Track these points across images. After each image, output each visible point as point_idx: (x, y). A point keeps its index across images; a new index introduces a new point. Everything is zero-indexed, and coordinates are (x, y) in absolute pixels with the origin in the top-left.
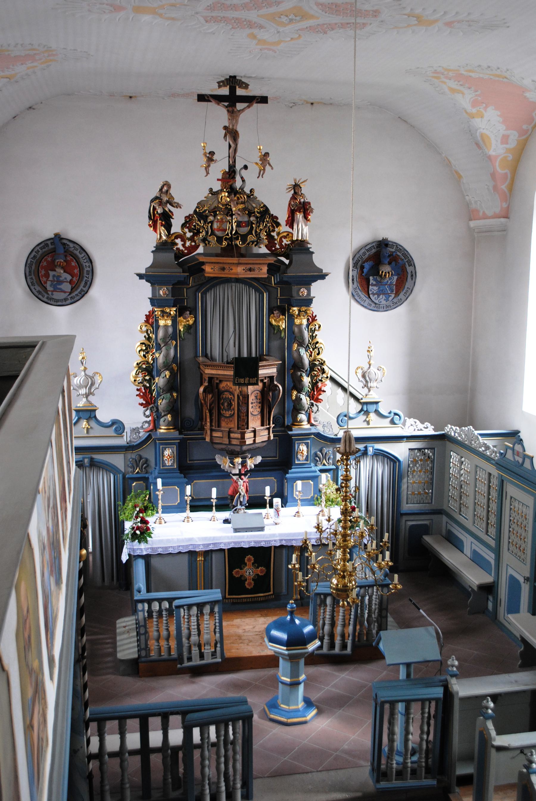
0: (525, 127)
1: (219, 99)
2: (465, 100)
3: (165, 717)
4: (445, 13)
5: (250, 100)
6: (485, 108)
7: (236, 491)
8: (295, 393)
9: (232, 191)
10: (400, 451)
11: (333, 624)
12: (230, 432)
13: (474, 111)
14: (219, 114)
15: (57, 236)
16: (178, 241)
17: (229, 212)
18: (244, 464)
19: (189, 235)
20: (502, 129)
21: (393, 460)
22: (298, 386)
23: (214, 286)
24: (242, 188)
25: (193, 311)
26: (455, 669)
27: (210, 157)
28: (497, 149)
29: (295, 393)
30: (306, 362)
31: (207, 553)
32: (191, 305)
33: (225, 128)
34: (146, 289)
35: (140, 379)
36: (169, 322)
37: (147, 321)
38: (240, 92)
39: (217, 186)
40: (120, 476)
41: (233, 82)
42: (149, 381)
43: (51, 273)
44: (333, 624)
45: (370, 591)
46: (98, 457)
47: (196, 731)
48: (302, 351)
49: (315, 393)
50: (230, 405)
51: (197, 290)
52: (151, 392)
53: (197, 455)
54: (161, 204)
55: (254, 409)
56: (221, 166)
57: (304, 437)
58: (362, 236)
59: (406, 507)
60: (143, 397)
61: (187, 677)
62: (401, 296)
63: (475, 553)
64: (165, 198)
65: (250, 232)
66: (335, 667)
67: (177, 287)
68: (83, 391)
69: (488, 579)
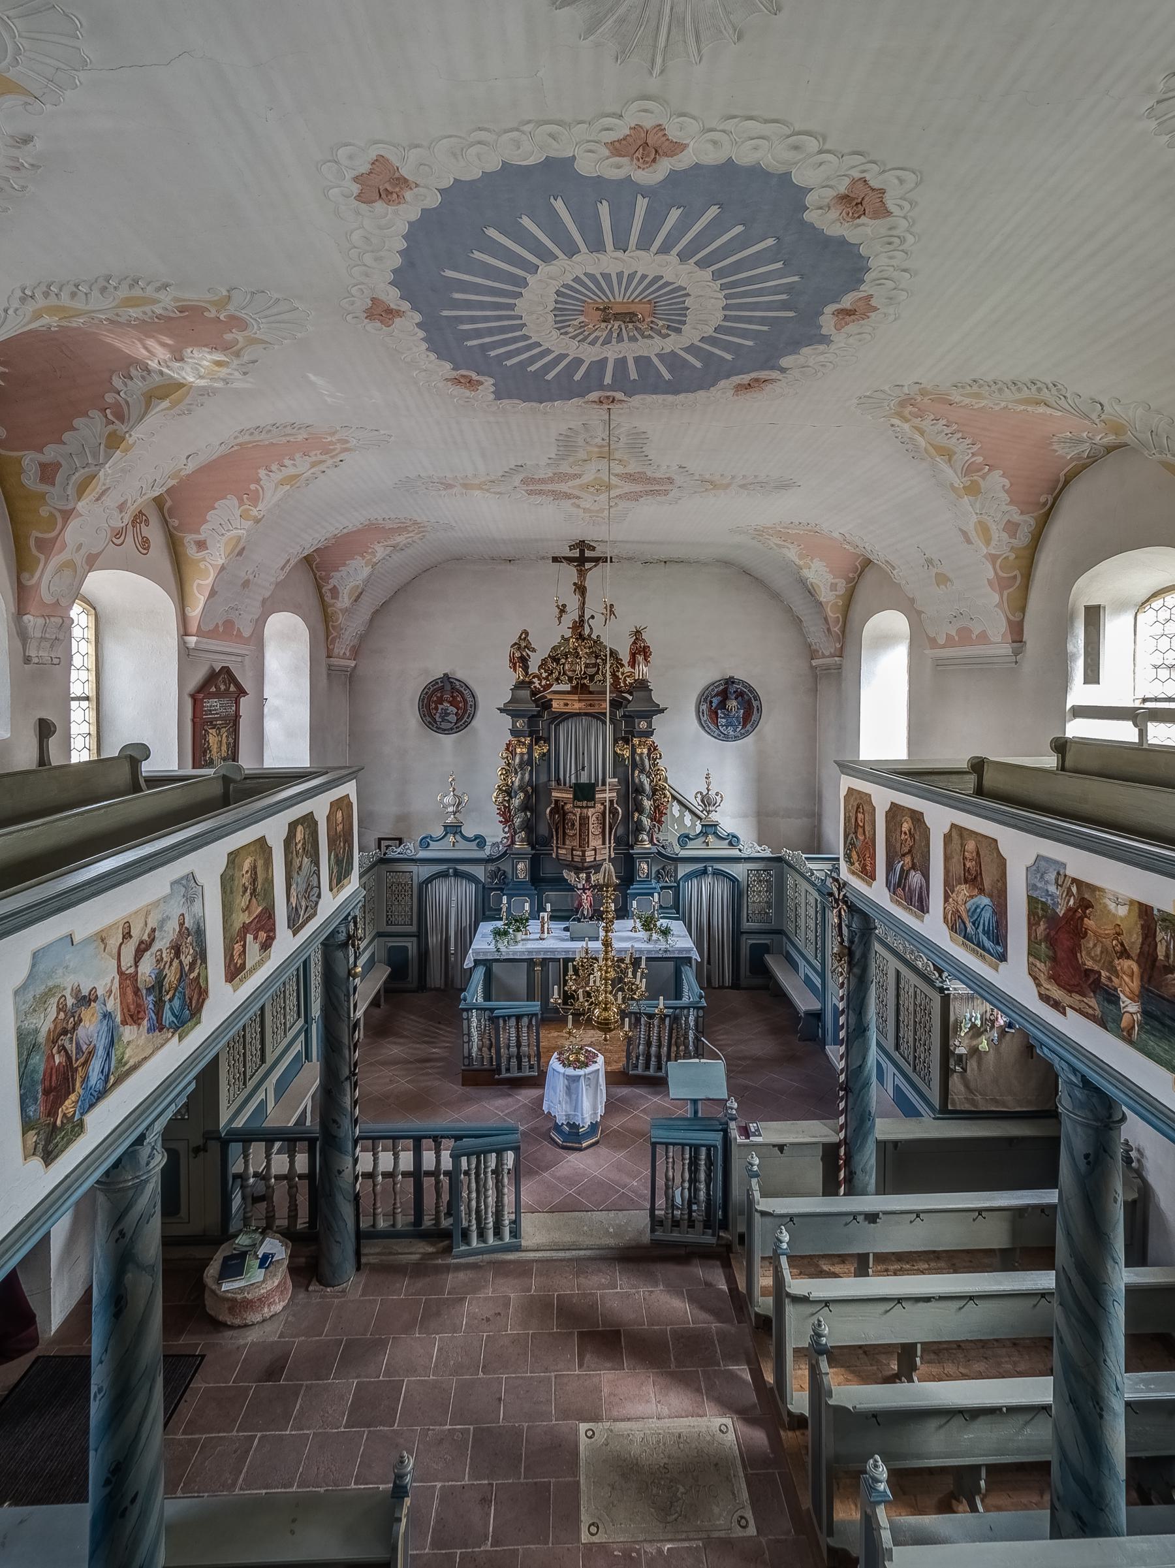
0: (851, 575)
1: (569, 560)
2: (792, 554)
3: (437, 1139)
4: (733, 477)
5: (596, 560)
6: (812, 560)
7: (580, 905)
8: (636, 815)
9: (581, 637)
10: (738, 871)
11: (649, 1044)
12: (573, 850)
13: (801, 563)
14: (570, 573)
15: (446, 675)
16: (535, 680)
17: (577, 656)
18: (588, 879)
19: (544, 675)
20: (830, 578)
21: (733, 880)
22: (640, 809)
23: (567, 718)
24: (589, 636)
25: (547, 740)
26: (734, 1112)
27: (562, 610)
28: (828, 596)
29: (636, 815)
30: (647, 787)
31: (544, 962)
32: (545, 736)
33: (575, 584)
34: (507, 721)
35: (500, 799)
36: (525, 750)
37: (507, 749)
38: (588, 554)
39: (568, 633)
40: (480, 886)
41: (582, 545)
42: (508, 801)
43: (440, 707)
44: (649, 1044)
45: (685, 1011)
46: (460, 867)
47: (464, 1160)
48: (643, 778)
49: (658, 815)
50: (573, 825)
51: (552, 723)
52: (510, 812)
53: (548, 871)
54: (519, 648)
55: (594, 828)
56: (572, 615)
57: (645, 856)
58: (705, 676)
59: (746, 925)
60: (503, 815)
61: (505, 1088)
62: (748, 727)
63: (806, 976)
64: (523, 644)
65: (597, 673)
66: (651, 1090)
67: (533, 719)
68: (451, 809)
69: (817, 1006)
